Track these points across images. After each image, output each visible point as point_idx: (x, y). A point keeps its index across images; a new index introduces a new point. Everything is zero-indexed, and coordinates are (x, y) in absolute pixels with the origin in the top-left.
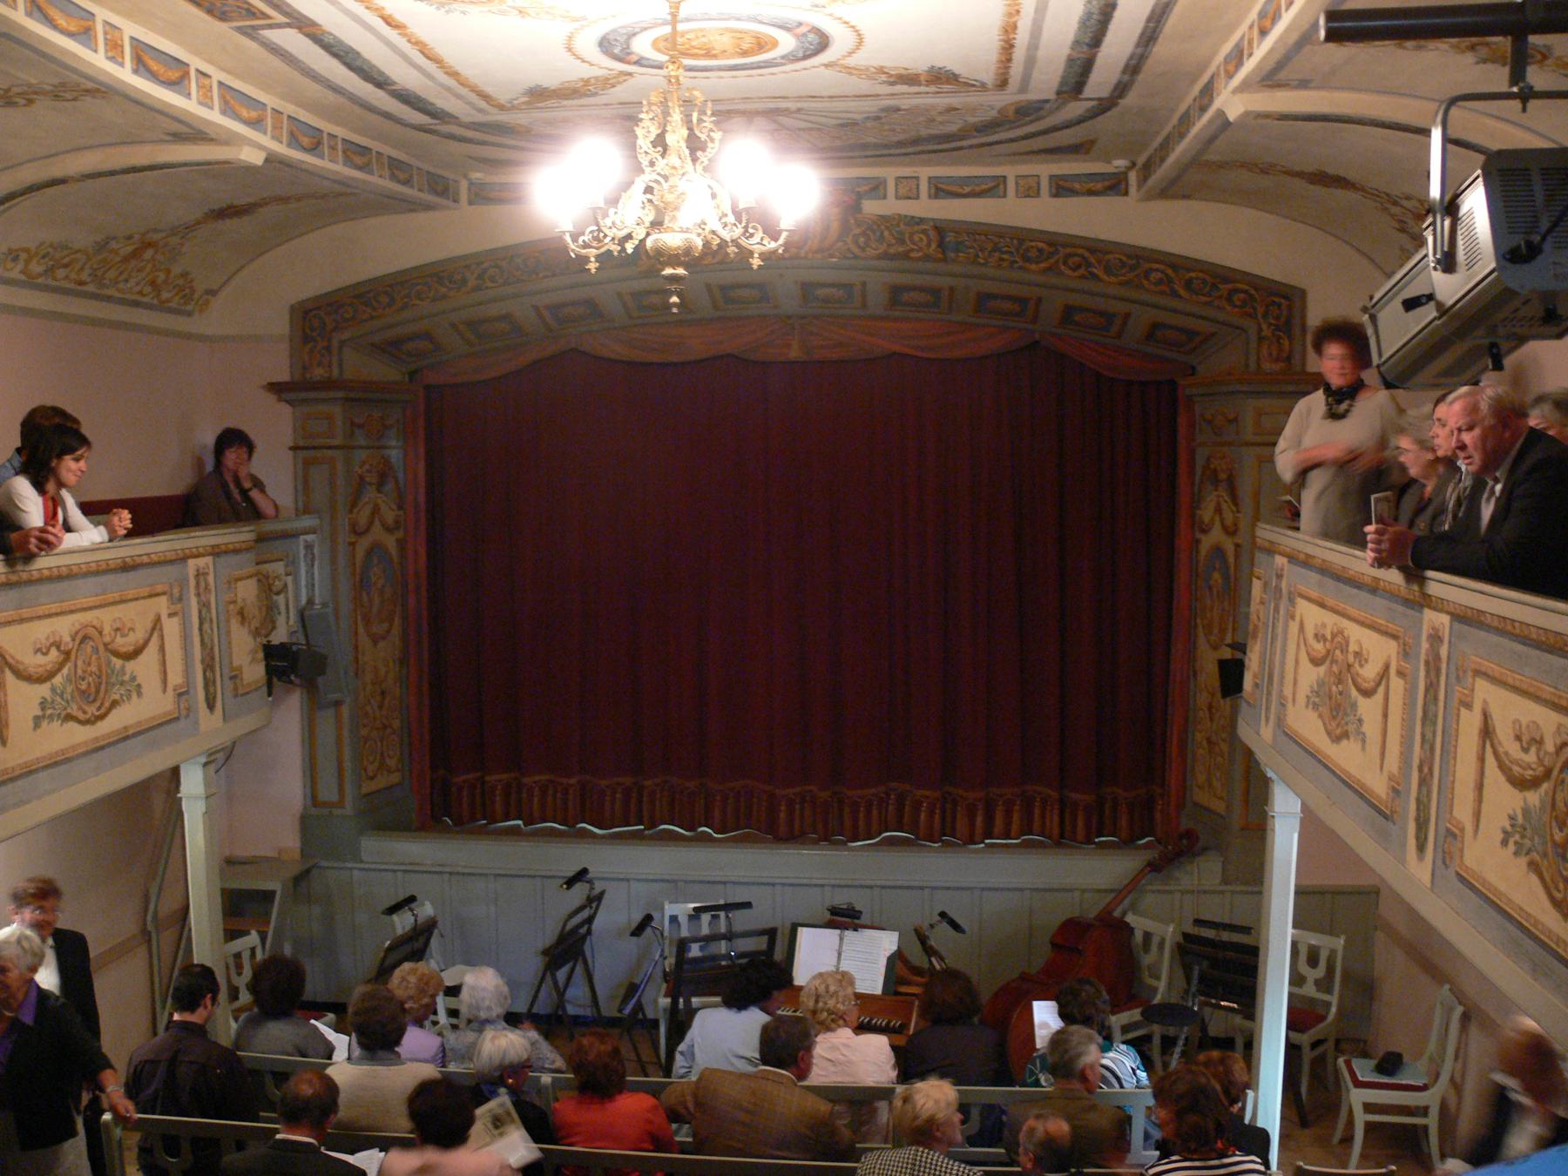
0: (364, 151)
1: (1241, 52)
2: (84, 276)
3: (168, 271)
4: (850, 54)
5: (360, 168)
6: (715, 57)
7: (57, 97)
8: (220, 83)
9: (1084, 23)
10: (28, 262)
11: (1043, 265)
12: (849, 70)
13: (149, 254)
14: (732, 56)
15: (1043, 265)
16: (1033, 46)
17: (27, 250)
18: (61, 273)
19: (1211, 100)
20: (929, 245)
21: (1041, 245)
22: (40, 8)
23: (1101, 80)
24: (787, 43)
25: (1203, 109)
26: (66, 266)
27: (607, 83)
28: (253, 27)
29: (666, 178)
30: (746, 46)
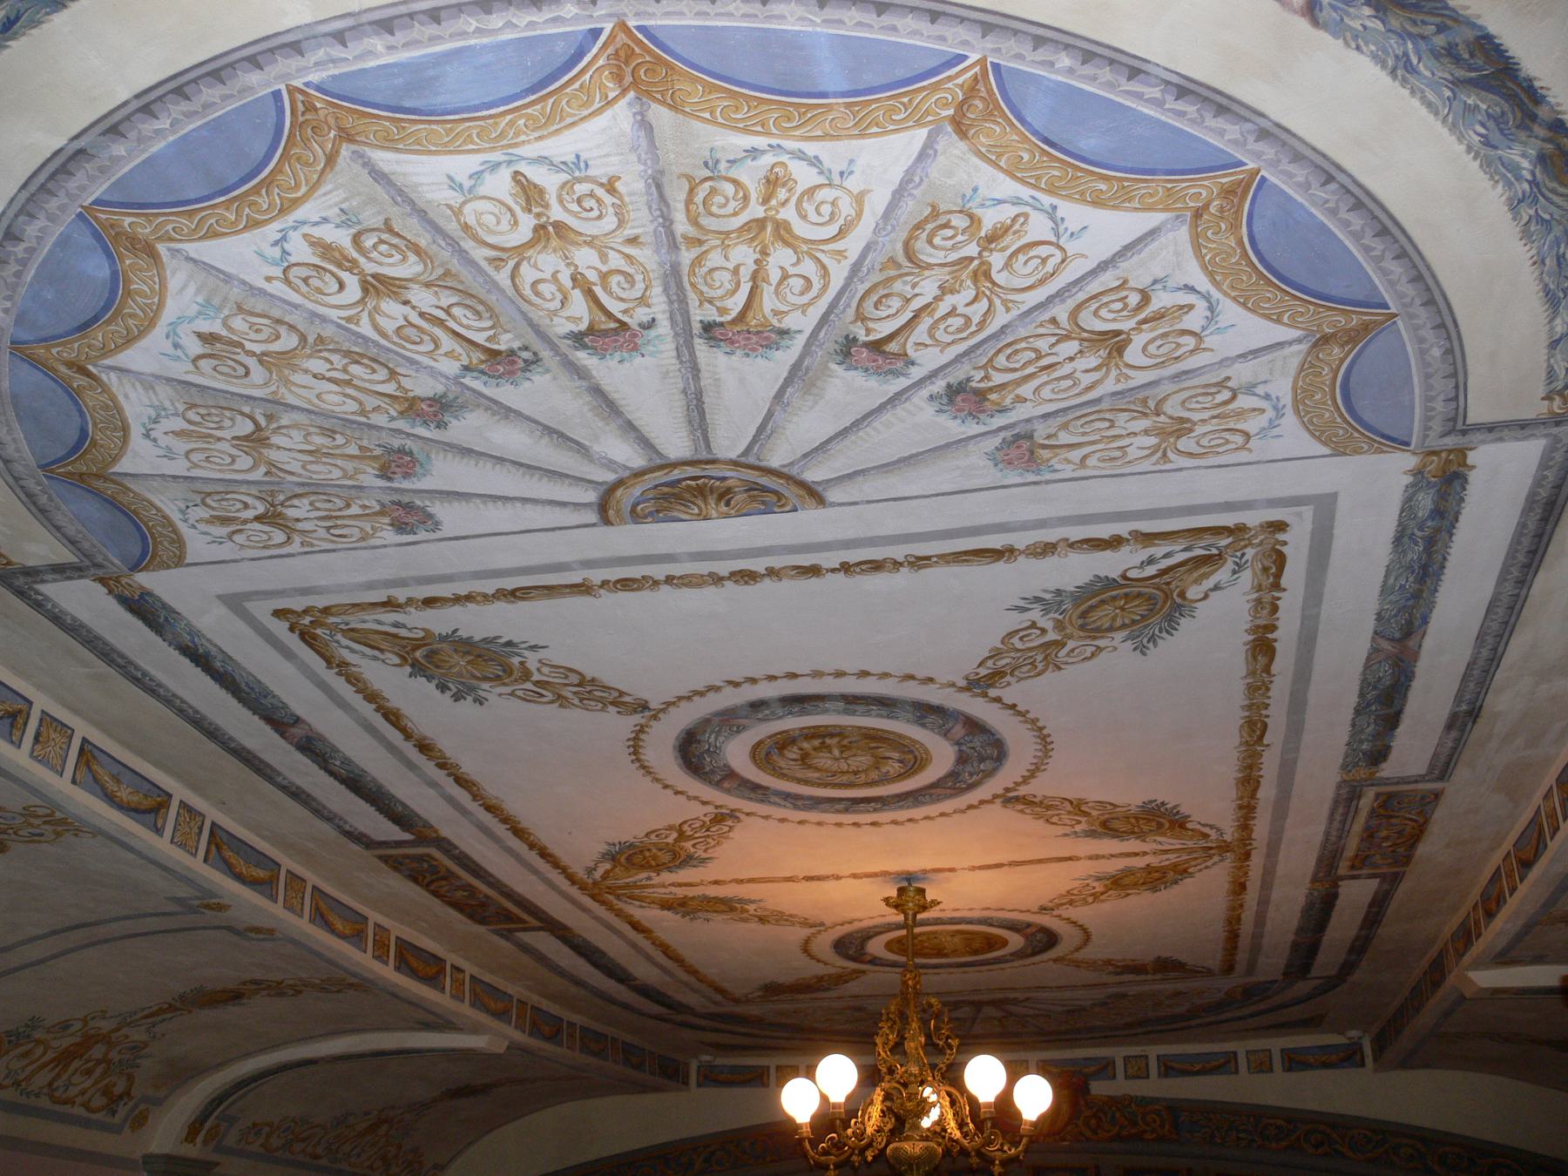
0: (599, 1036)
1: (1469, 933)
2: (319, 1150)
3: (400, 1147)
4: (1077, 950)
5: (595, 1054)
6: (946, 956)
7: (323, 989)
8: (472, 977)
9: (1307, 910)
10: (268, 1136)
11: (1284, 1143)
12: (1078, 964)
13: (384, 1128)
14: (963, 955)
15: (1284, 1143)
16: (1257, 936)
17: (270, 1125)
18: (298, 1147)
19: (1443, 977)
20: (1162, 1126)
21: (1280, 1122)
22: (322, 916)
23: (1329, 957)
24: (1016, 941)
25: (1436, 984)
26: (303, 1140)
27: (840, 979)
28: (509, 930)
29: (905, 1085)
30: (976, 945)
